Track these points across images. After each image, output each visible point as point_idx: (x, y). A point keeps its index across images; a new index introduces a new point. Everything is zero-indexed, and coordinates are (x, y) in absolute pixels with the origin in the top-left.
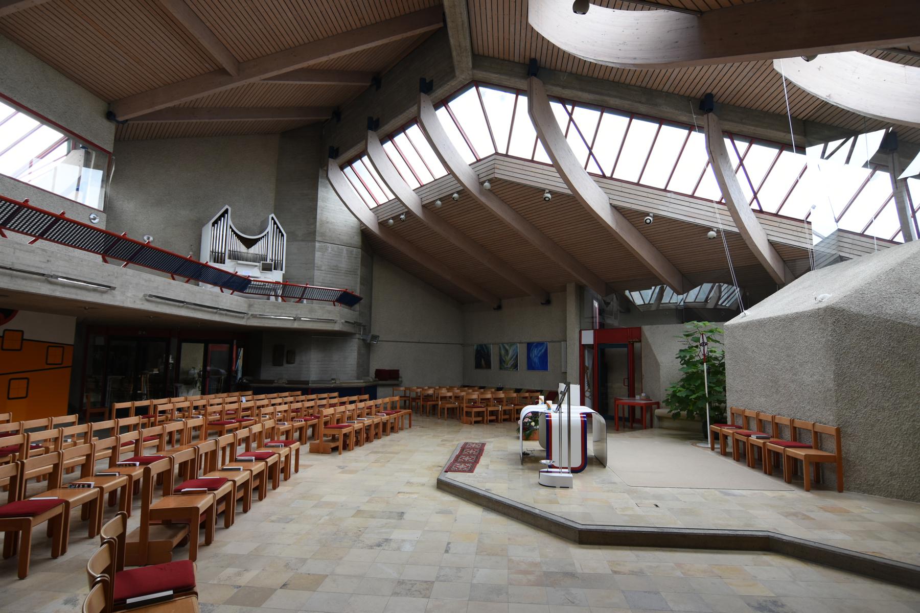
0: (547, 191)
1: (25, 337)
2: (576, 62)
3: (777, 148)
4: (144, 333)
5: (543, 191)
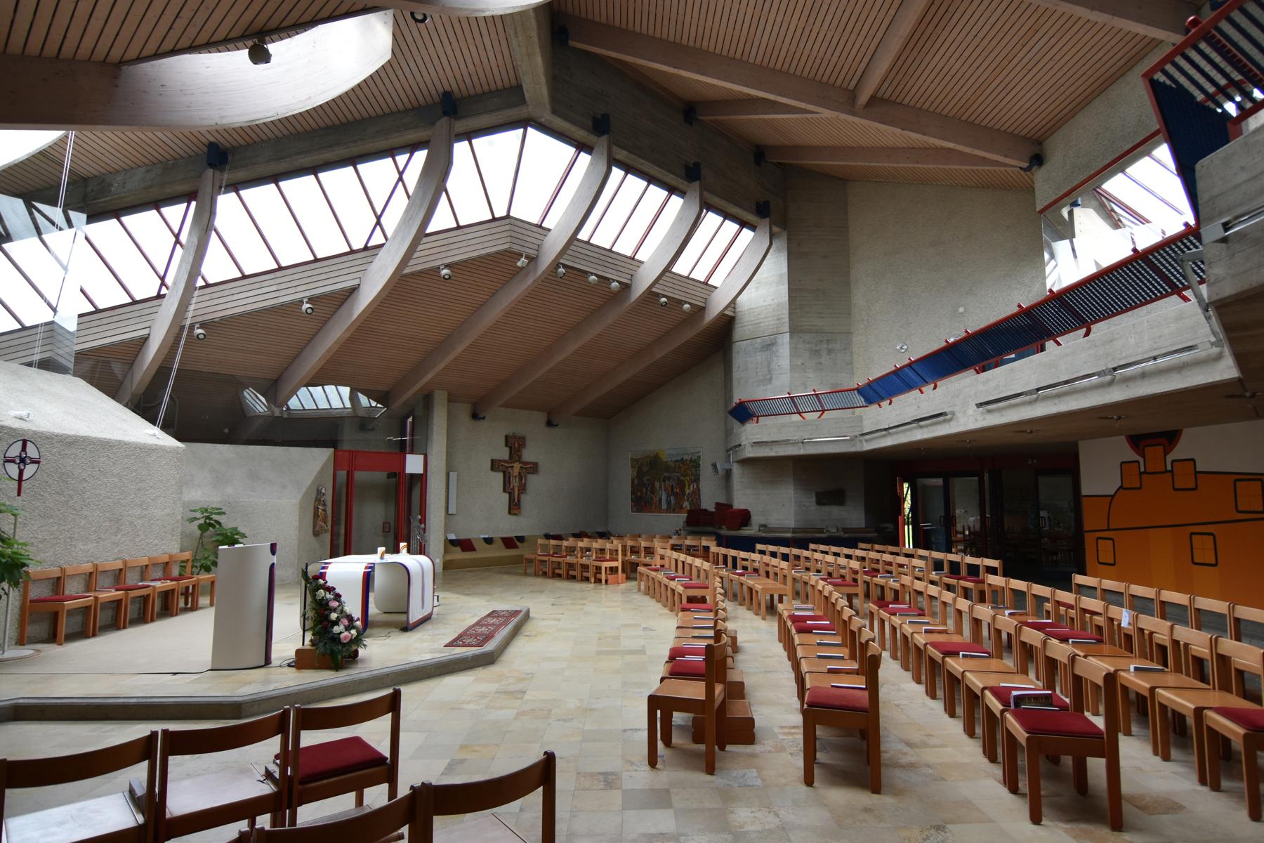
0: (197, 326)
1: (1198, 469)
2: (359, 92)
4: (1035, 461)
5: (438, 269)
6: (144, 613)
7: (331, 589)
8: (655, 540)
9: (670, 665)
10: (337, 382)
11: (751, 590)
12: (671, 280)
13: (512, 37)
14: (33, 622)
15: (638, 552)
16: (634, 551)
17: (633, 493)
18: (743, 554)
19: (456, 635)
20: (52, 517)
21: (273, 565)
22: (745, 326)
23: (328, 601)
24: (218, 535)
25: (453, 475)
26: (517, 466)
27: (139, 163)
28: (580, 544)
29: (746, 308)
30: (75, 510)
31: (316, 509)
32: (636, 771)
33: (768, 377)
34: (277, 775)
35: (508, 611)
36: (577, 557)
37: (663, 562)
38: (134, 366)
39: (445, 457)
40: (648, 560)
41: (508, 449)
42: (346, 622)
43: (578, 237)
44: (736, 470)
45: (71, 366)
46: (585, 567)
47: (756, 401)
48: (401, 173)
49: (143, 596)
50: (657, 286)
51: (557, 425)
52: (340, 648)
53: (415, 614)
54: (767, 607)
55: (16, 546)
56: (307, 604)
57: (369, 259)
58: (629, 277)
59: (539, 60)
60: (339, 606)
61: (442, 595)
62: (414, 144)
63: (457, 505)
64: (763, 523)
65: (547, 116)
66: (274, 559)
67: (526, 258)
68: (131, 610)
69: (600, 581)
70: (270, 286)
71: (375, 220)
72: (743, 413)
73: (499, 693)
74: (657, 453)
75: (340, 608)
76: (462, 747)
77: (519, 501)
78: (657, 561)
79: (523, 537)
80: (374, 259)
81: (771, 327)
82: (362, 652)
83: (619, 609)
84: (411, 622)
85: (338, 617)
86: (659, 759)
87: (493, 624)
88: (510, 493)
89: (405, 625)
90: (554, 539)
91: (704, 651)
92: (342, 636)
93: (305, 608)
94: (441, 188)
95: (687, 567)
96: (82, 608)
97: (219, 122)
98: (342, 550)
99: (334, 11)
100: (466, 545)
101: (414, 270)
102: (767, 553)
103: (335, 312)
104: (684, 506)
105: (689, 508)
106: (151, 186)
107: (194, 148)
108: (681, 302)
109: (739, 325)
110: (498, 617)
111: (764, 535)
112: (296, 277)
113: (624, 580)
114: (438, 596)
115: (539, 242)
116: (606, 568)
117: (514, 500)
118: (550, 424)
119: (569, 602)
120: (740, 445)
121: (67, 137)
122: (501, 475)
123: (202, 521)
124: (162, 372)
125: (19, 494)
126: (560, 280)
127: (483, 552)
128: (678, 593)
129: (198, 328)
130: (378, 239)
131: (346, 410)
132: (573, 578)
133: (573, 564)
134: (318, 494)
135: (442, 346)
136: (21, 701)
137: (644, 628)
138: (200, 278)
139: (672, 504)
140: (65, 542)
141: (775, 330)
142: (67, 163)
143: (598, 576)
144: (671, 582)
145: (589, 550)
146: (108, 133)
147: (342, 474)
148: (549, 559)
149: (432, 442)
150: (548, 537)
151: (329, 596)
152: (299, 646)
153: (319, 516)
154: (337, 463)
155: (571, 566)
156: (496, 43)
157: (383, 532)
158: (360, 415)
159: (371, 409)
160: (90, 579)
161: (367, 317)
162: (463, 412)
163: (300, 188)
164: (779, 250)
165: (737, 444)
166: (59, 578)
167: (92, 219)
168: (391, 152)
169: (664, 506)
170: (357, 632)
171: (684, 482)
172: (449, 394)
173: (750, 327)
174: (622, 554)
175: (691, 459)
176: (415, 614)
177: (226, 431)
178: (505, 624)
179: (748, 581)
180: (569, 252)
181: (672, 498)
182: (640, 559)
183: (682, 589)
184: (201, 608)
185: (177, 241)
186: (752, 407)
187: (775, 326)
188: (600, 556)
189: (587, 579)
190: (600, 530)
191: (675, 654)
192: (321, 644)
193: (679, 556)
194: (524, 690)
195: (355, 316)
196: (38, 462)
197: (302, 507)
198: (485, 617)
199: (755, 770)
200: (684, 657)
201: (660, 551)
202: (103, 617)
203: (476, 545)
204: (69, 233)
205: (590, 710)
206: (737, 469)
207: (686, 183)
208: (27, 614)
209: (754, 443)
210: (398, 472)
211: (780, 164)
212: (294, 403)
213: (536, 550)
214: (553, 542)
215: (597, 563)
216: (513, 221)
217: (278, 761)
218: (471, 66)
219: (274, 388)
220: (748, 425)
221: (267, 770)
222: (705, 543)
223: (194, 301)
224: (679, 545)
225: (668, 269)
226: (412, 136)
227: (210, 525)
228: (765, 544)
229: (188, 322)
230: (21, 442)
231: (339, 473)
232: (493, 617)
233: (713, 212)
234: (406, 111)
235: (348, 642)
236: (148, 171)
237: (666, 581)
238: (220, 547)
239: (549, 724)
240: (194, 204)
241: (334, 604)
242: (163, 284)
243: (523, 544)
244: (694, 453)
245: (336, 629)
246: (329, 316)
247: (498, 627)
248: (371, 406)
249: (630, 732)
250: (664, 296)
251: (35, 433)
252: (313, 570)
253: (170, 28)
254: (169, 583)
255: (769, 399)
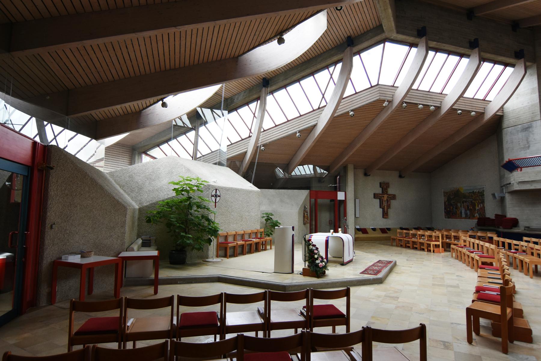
0: (262, 146)
3: (357, 55)
5: (348, 112)
6: (243, 252)
7: (314, 246)
8: (459, 232)
9: (477, 295)
10: (308, 164)
11: (521, 261)
12: (463, 101)
13: (377, 4)
14: (220, 250)
15: (450, 238)
16: (448, 237)
17: (445, 209)
18: (515, 242)
19: (364, 269)
20: (224, 215)
21: (293, 235)
22: (510, 120)
23: (313, 250)
24: (271, 223)
25: (357, 201)
26: (386, 196)
27: (242, 90)
28: (419, 233)
29: (510, 110)
30: (230, 213)
31: (304, 214)
32: (461, 343)
33: (527, 146)
34: (305, 314)
35: (386, 261)
36: (417, 239)
37: (465, 244)
38: (243, 162)
39: (353, 193)
40: (456, 242)
41: (381, 189)
42: (320, 259)
43: (412, 88)
44: (508, 197)
45: (226, 164)
46: (422, 244)
47: (520, 159)
48: (331, 75)
49: (250, 244)
50: (456, 105)
51: (404, 177)
52: (319, 269)
53: (346, 259)
54: (533, 272)
55: (215, 224)
56: (306, 251)
57: (320, 112)
58: (440, 103)
59: (390, 11)
60: (318, 252)
61: (356, 252)
62: (336, 62)
63: (359, 213)
64: (527, 225)
65: (394, 35)
66: (293, 233)
67: (387, 102)
68: (247, 249)
69: (430, 251)
70: (285, 127)
71: (322, 96)
72: (511, 166)
73: (386, 296)
74: (458, 189)
75: (318, 253)
76: (372, 317)
77: (387, 212)
78: (462, 243)
79: (390, 228)
80: (322, 112)
81: (527, 118)
82: (327, 272)
83: (441, 265)
84: (345, 262)
85: (318, 257)
86: (473, 340)
87: (380, 266)
88: (383, 208)
89: (342, 263)
90: (405, 230)
91: (499, 290)
92: (319, 264)
93: (305, 252)
94: (348, 78)
95: (480, 247)
96: (233, 246)
97: (268, 70)
98: (314, 231)
99: (306, 16)
100: (364, 231)
101: (338, 114)
102: (531, 242)
103: (308, 136)
104: (475, 216)
105: (478, 217)
106: (246, 98)
107: (259, 81)
108: (470, 112)
109: (507, 119)
110: (382, 263)
111: (528, 232)
112: (295, 123)
113: (443, 251)
114: (355, 252)
115: (393, 94)
116: (433, 245)
117: (385, 212)
118: (400, 176)
119: (415, 259)
120: (510, 184)
121: (222, 86)
122: (378, 200)
123: (266, 218)
124: (252, 163)
125: (215, 207)
126: (404, 109)
127: (372, 234)
128: (476, 259)
129: (262, 147)
130: (323, 104)
131: (312, 175)
132: (416, 249)
133: (415, 242)
134: (304, 208)
135: (351, 145)
136: (220, 276)
137: (457, 275)
138: (262, 129)
139: (468, 214)
140: (228, 224)
141: (530, 119)
142: (223, 95)
143: (429, 248)
144: (471, 254)
145: (423, 236)
146: (231, 83)
147: (313, 200)
148: (403, 239)
149: (348, 186)
150: (402, 229)
151: (314, 248)
152: (304, 267)
153: (305, 217)
154: (311, 196)
155: (414, 243)
156: (369, 9)
157: (329, 224)
158: (317, 176)
159: (321, 174)
160: (235, 236)
161: (321, 136)
162: (360, 173)
163: (294, 88)
164: (531, 75)
165: (508, 183)
166: (226, 236)
167: (229, 112)
168: (327, 67)
169: (464, 216)
170: (325, 263)
171: (475, 204)
172: (354, 166)
173: (513, 120)
174: (442, 239)
175: (479, 192)
176: (346, 259)
177: (272, 184)
178: (386, 266)
179: (519, 256)
180: (408, 96)
181: (468, 212)
182: (452, 242)
183: (479, 257)
184: (267, 250)
185: (254, 116)
186: (517, 163)
187: (531, 117)
188: (429, 239)
189: (423, 250)
190: (428, 226)
191: (479, 290)
192: (312, 267)
193: (475, 241)
194: (398, 297)
195: (316, 136)
196: (220, 196)
197: (299, 213)
198: (376, 263)
199: (534, 357)
200: (485, 292)
201: (463, 238)
202: (239, 250)
203: (368, 231)
204: (223, 118)
205: (432, 310)
206: (508, 196)
207: (470, 50)
208: (219, 247)
209: (519, 182)
210: (334, 199)
211: (529, 27)
212: (293, 173)
213: (397, 234)
214: (405, 231)
215: (429, 242)
216: (380, 86)
217: (305, 309)
218: (359, 22)
219: (287, 167)
220: (515, 173)
221: (301, 311)
222: (489, 235)
223: (261, 136)
224: (473, 236)
225: (461, 96)
226: (335, 58)
227: (269, 219)
228: (530, 237)
229: (259, 145)
230: (215, 190)
231: (311, 200)
232: (380, 263)
233: (487, 62)
234: (333, 48)
235: (322, 267)
236: (245, 93)
237: (468, 253)
238: (276, 227)
239: (412, 314)
240: (259, 101)
241: (316, 252)
242: (251, 132)
243: (390, 232)
244: (480, 188)
245: (317, 262)
246: (306, 137)
247: (383, 267)
248: (321, 173)
249: (455, 324)
250: (459, 110)
251: (218, 187)
252: (307, 237)
253: (253, 40)
254: (258, 240)
255: (529, 158)
